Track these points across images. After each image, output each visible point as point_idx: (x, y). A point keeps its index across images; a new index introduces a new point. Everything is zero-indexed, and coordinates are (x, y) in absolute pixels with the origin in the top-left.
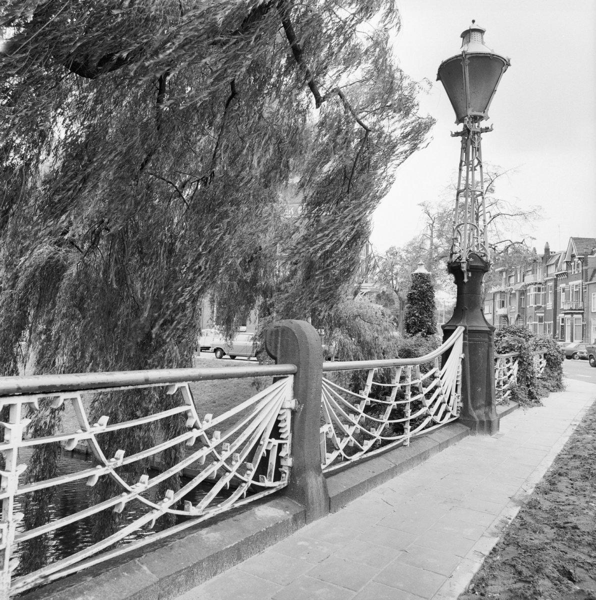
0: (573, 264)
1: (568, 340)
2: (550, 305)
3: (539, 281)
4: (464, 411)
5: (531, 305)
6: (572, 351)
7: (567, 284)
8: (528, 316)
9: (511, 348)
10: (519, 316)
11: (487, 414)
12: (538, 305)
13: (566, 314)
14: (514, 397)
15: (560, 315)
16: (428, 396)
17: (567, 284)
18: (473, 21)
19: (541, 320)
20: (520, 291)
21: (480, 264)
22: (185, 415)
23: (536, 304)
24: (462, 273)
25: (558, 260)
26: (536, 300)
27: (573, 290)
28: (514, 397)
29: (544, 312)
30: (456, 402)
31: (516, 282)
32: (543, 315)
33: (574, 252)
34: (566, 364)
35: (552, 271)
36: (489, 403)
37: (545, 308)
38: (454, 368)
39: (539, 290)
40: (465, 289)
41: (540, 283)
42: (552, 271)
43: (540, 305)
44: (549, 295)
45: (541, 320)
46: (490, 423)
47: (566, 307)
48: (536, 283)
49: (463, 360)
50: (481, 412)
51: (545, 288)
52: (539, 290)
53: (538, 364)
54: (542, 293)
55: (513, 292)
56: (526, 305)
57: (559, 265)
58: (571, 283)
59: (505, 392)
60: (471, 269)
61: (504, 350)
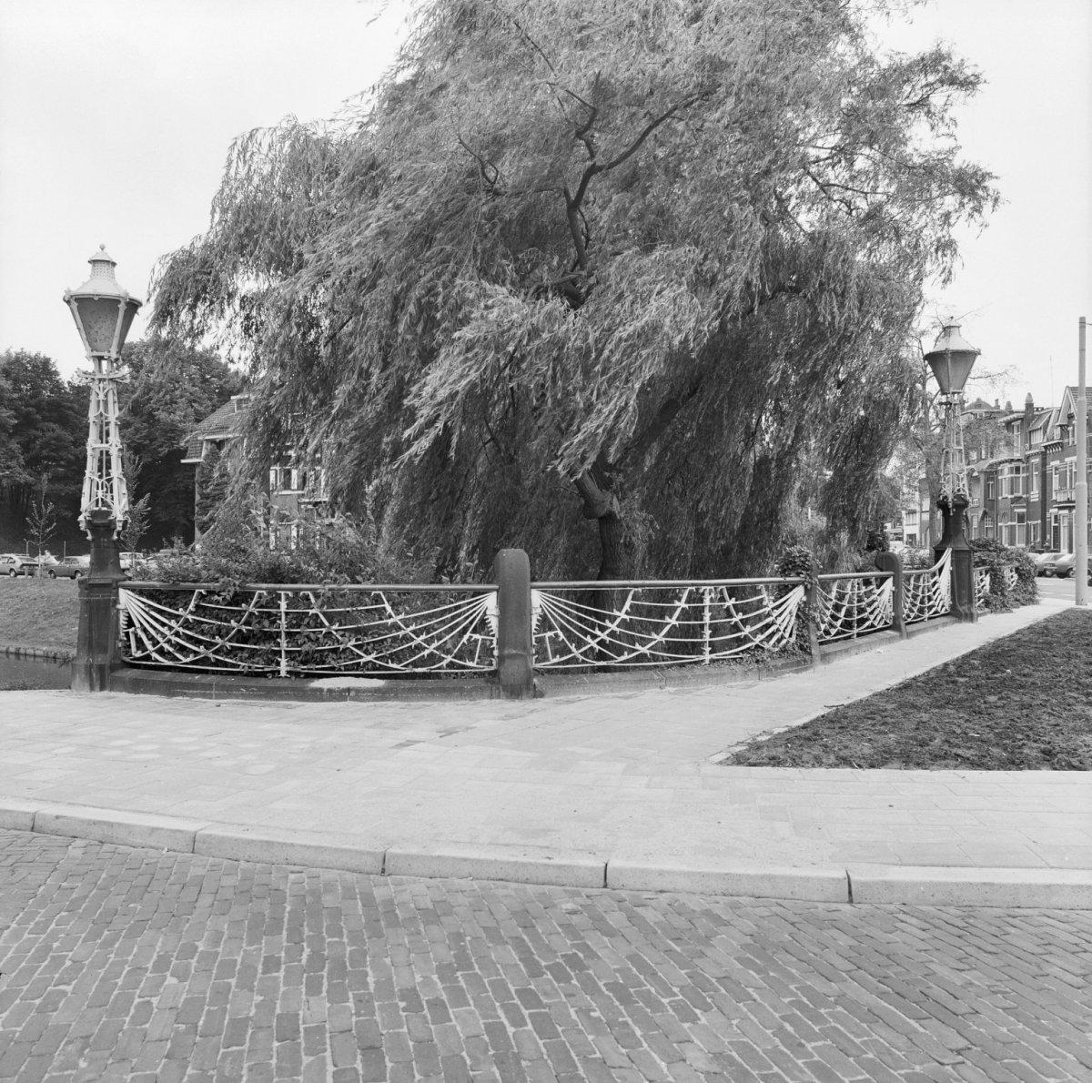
0: (1070, 428)
1: (1064, 550)
2: (1035, 495)
3: (1017, 455)
4: (953, 607)
5: (1005, 495)
6: (1066, 566)
7: (1062, 461)
8: (1002, 512)
9: (983, 563)
10: (985, 513)
11: (969, 609)
12: (1016, 494)
13: (1060, 508)
14: (987, 604)
15: (1051, 511)
16: (872, 613)
17: (1062, 461)
18: (947, 330)
19: (1021, 518)
20: (986, 472)
21: (962, 502)
22: (762, 600)
23: (1012, 493)
24: (949, 510)
25: (1048, 421)
26: (1012, 486)
27: (1071, 471)
28: (987, 604)
29: (1027, 507)
30: (947, 601)
31: (980, 459)
32: (1024, 510)
33: (1072, 411)
34: (1040, 581)
35: (1038, 439)
36: (970, 602)
37: (1027, 500)
38: (944, 580)
39: (1018, 470)
40: (951, 521)
41: (1018, 460)
42: (1038, 439)
43: (1020, 494)
44: (1035, 478)
45: (1021, 518)
46: (972, 614)
47: (1060, 497)
48: (1012, 460)
49: (952, 572)
50: (965, 608)
51: (1028, 468)
52: (1018, 470)
53: (1010, 577)
54: (1022, 475)
55: (975, 474)
56: (997, 495)
57: (1048, 431)
58: (1068, 460)
59: (980, 598)
60: (955, 506)
61: (977, 564)
